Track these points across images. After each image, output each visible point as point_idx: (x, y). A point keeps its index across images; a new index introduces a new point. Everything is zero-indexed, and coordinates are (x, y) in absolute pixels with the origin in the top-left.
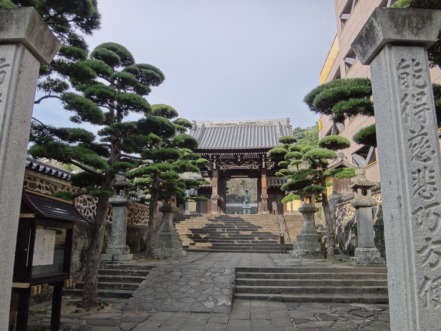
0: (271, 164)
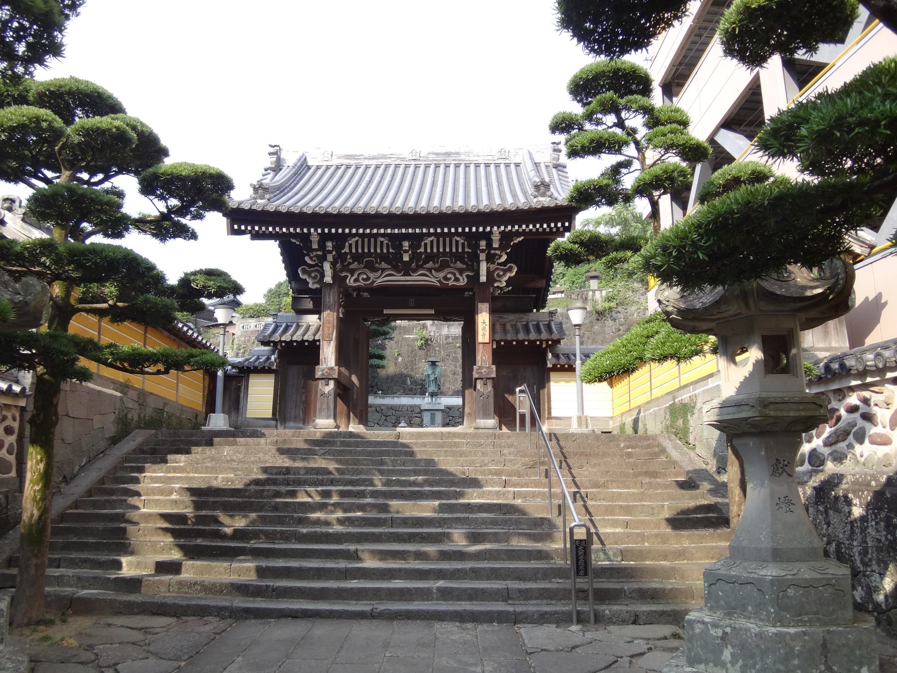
0: (505, 271)
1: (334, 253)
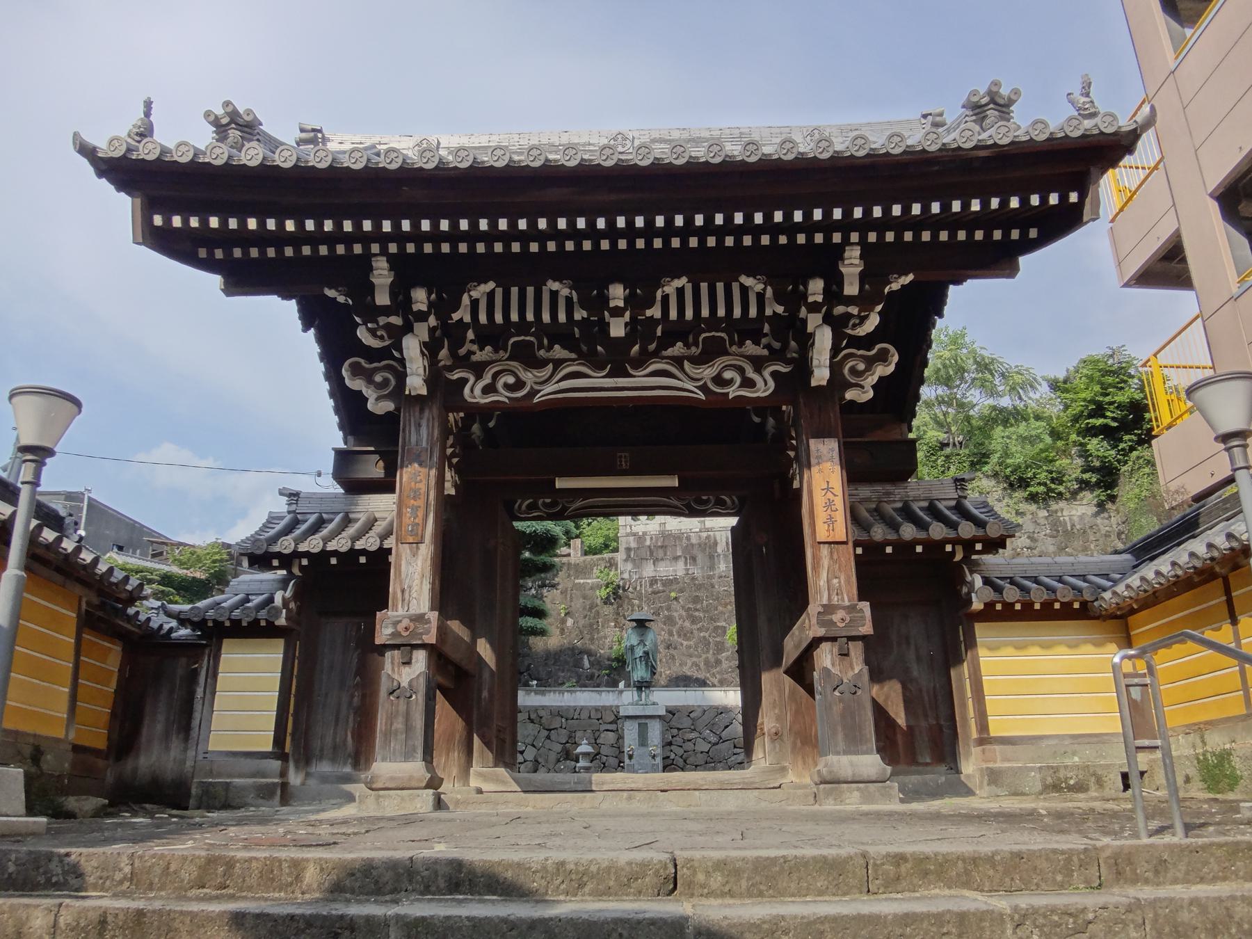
0: (870, 362)
1: (432, 321)
